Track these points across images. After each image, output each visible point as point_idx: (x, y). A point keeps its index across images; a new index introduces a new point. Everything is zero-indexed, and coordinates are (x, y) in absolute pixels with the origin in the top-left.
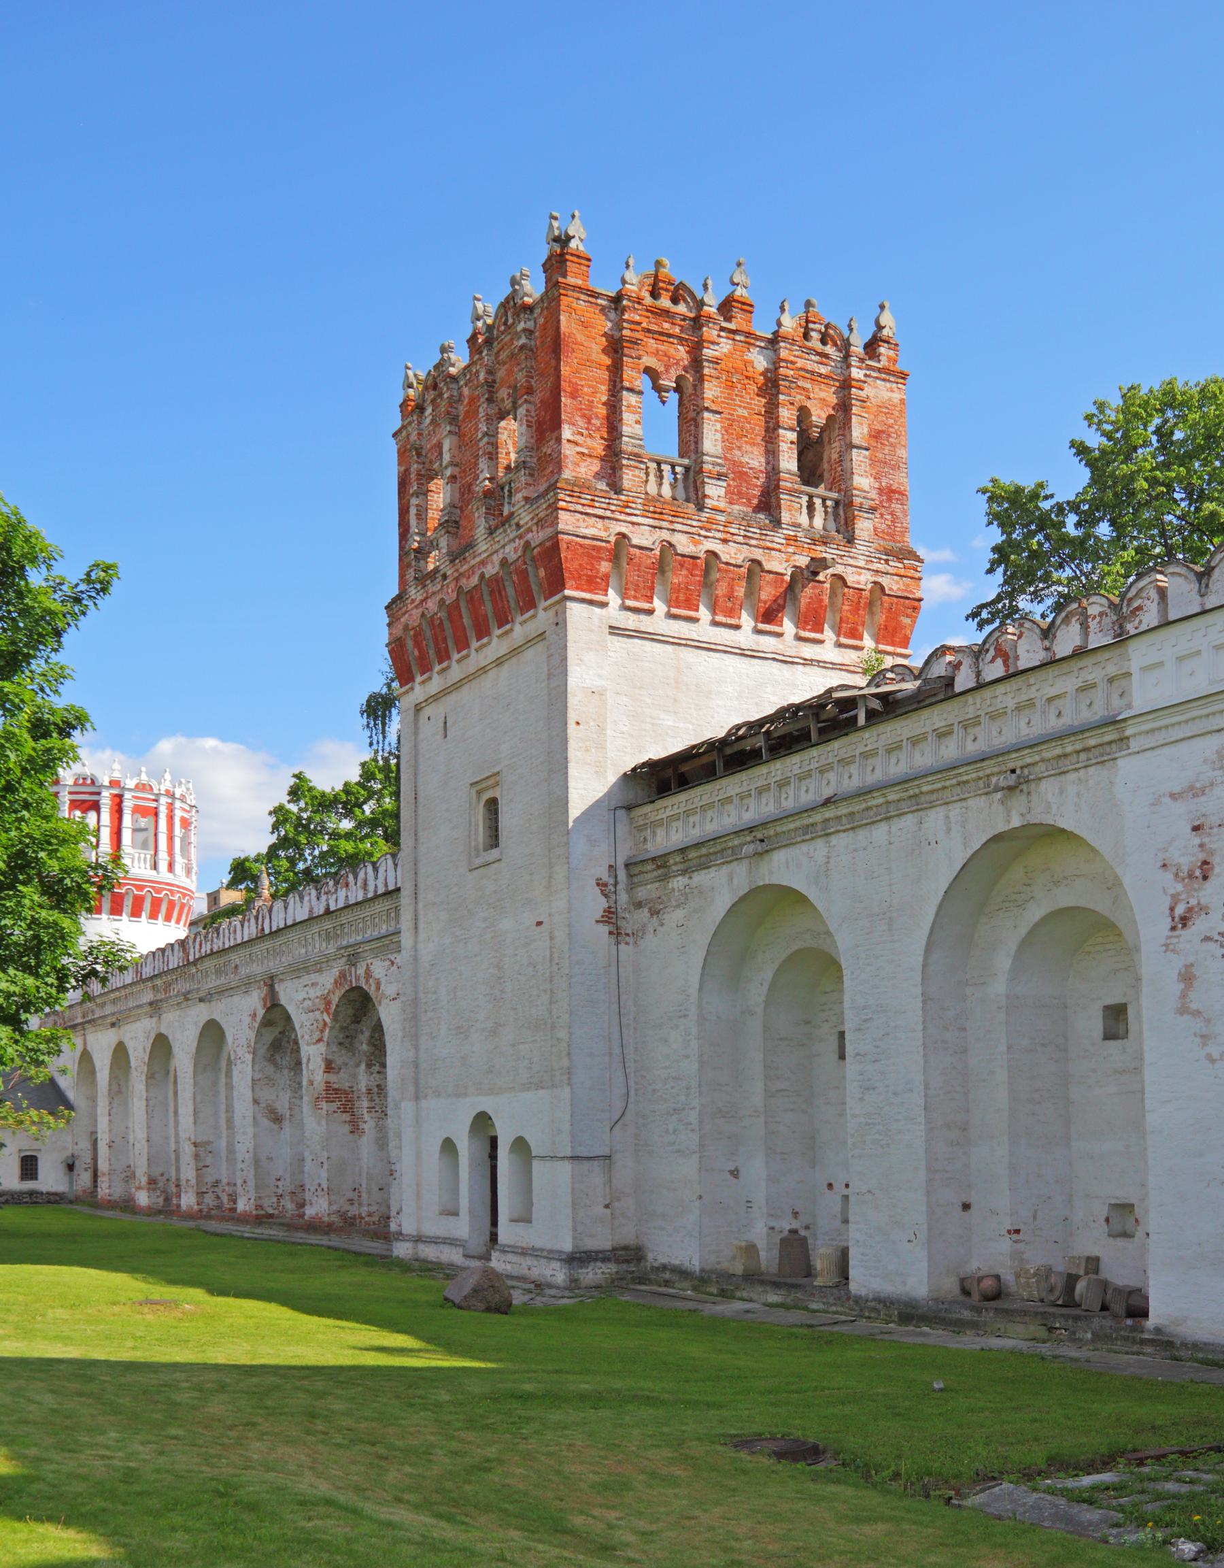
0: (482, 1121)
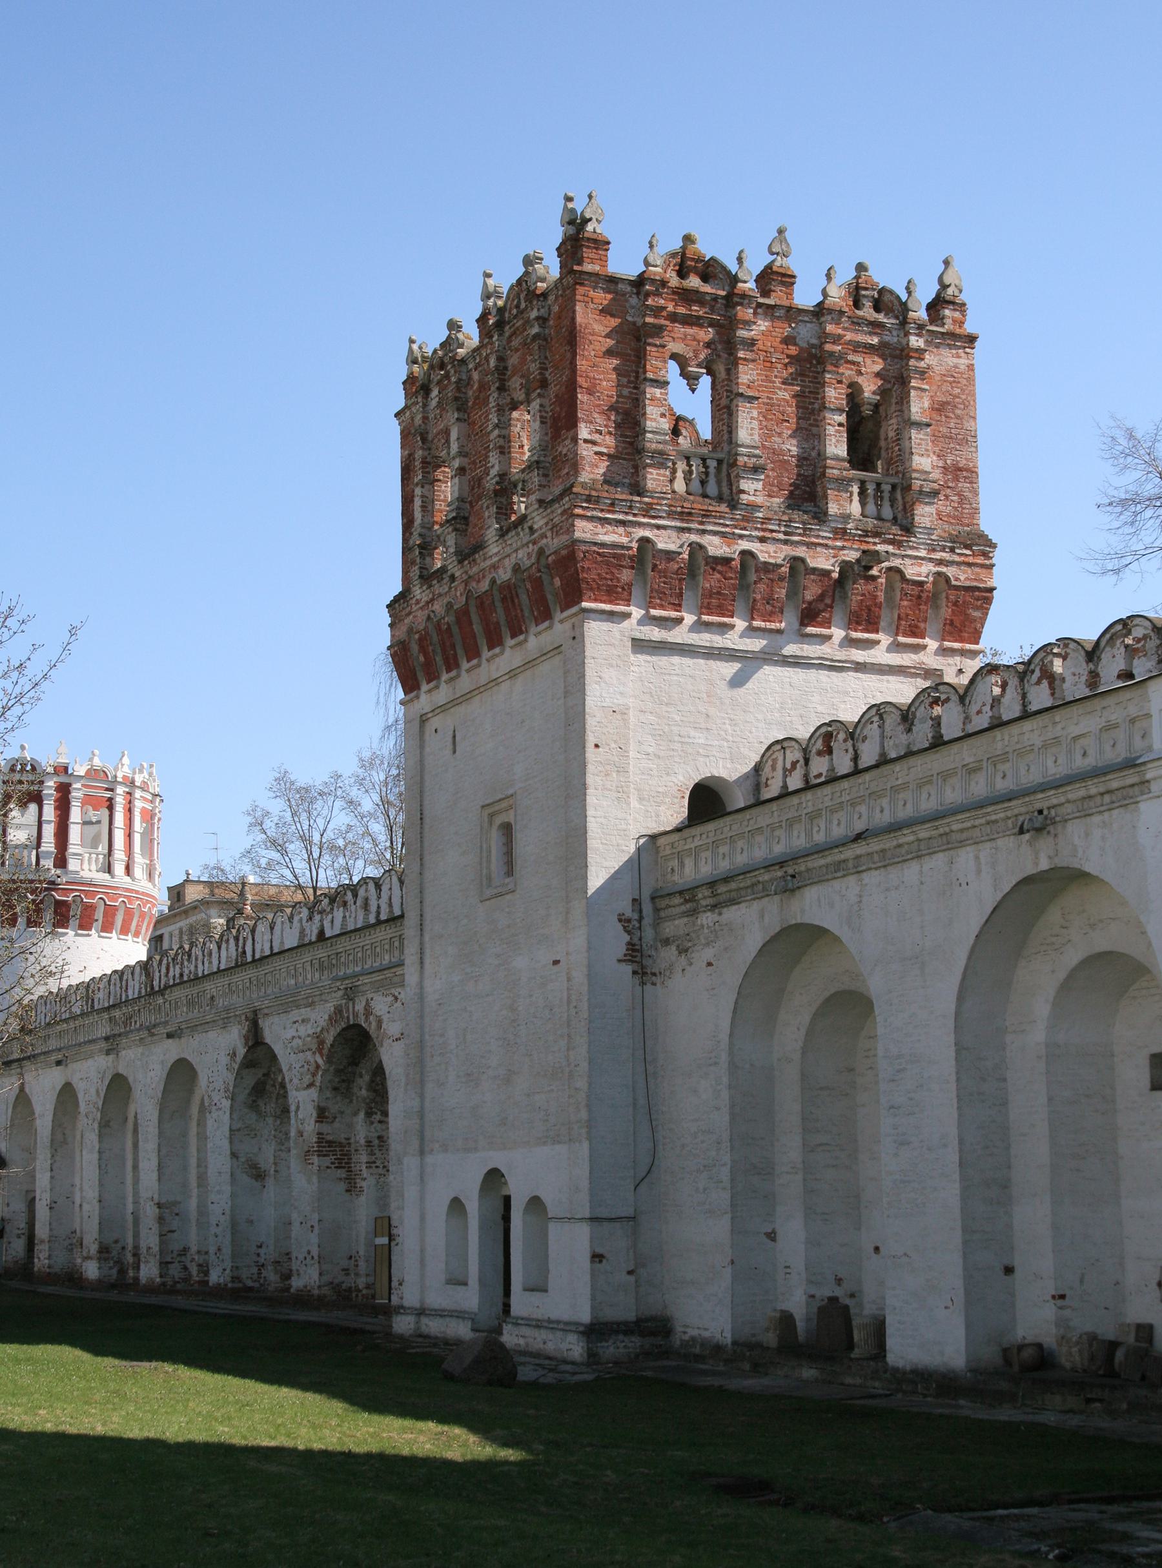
0: (494, 1177)
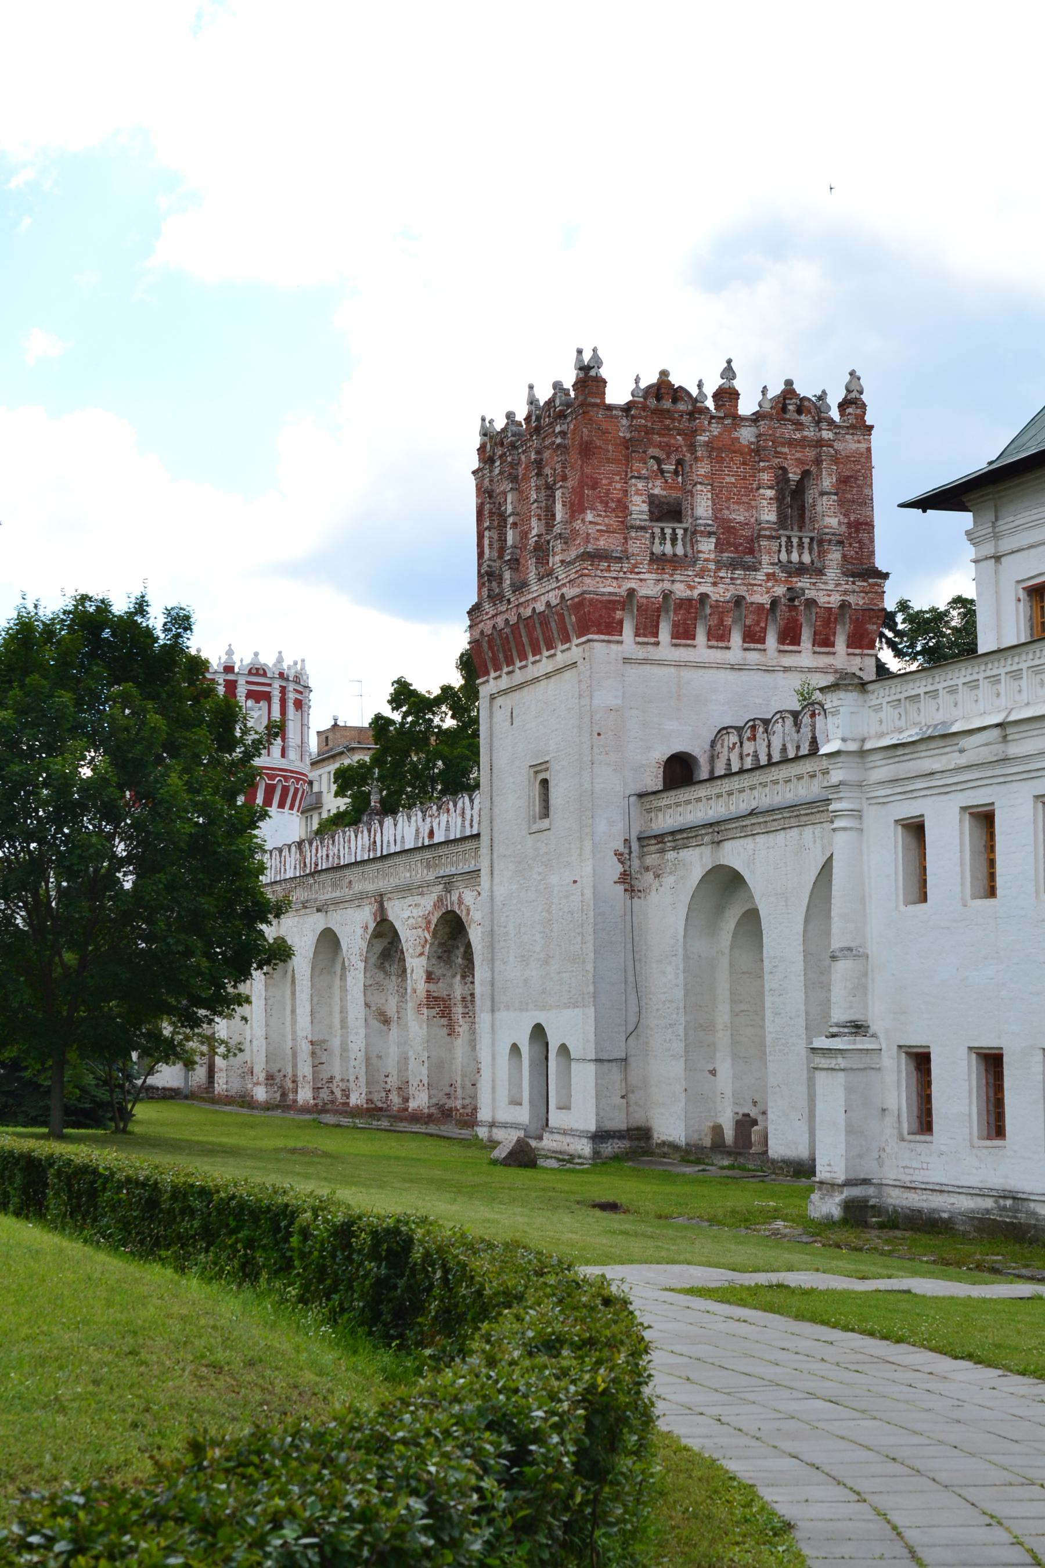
0: (539, 1032)
